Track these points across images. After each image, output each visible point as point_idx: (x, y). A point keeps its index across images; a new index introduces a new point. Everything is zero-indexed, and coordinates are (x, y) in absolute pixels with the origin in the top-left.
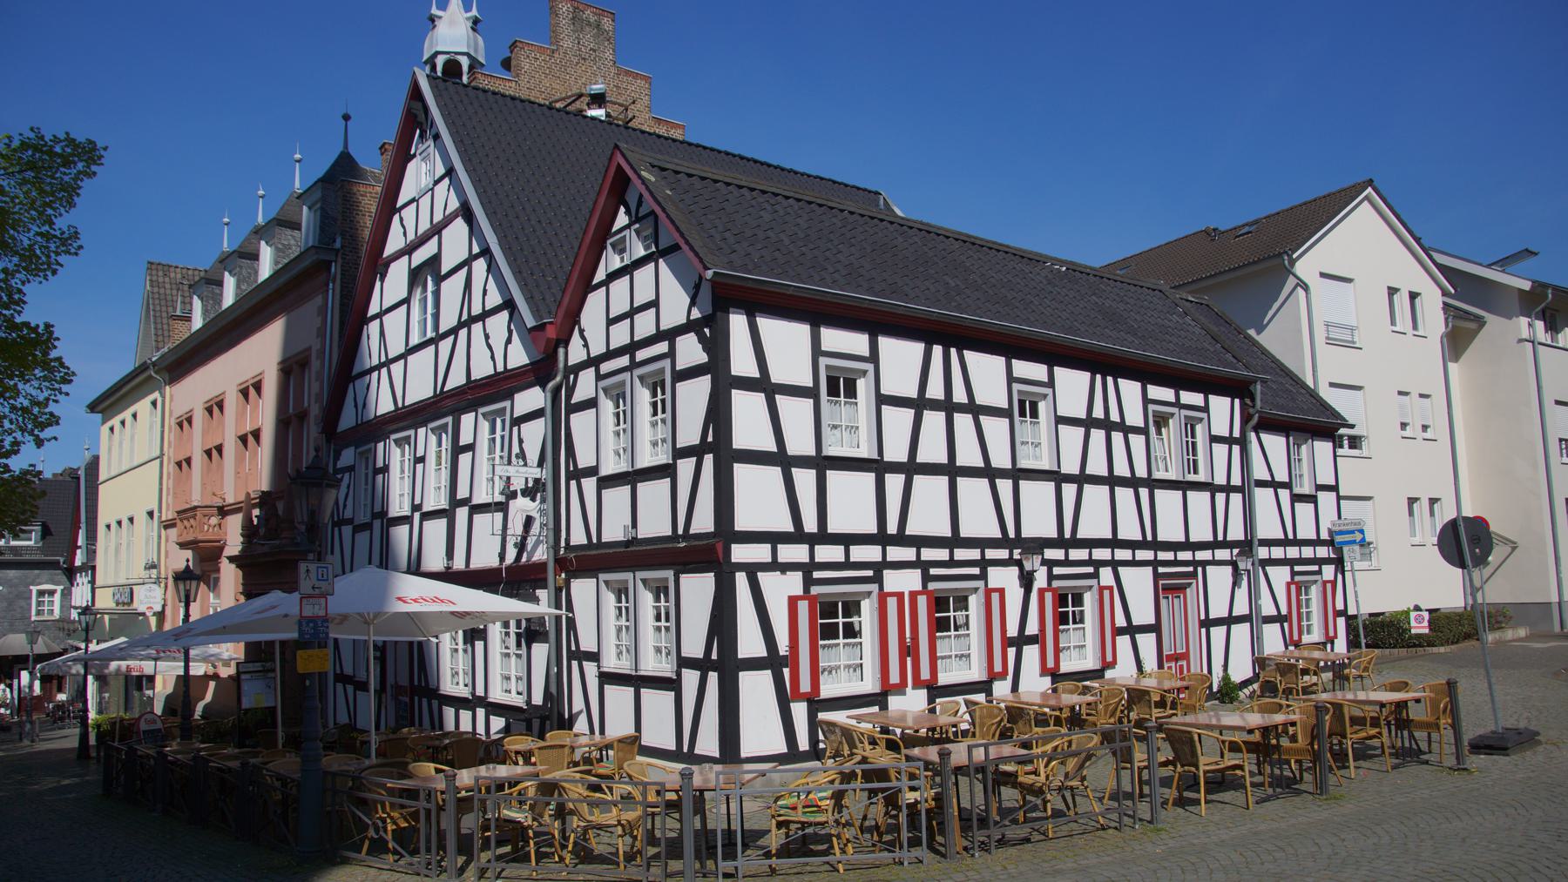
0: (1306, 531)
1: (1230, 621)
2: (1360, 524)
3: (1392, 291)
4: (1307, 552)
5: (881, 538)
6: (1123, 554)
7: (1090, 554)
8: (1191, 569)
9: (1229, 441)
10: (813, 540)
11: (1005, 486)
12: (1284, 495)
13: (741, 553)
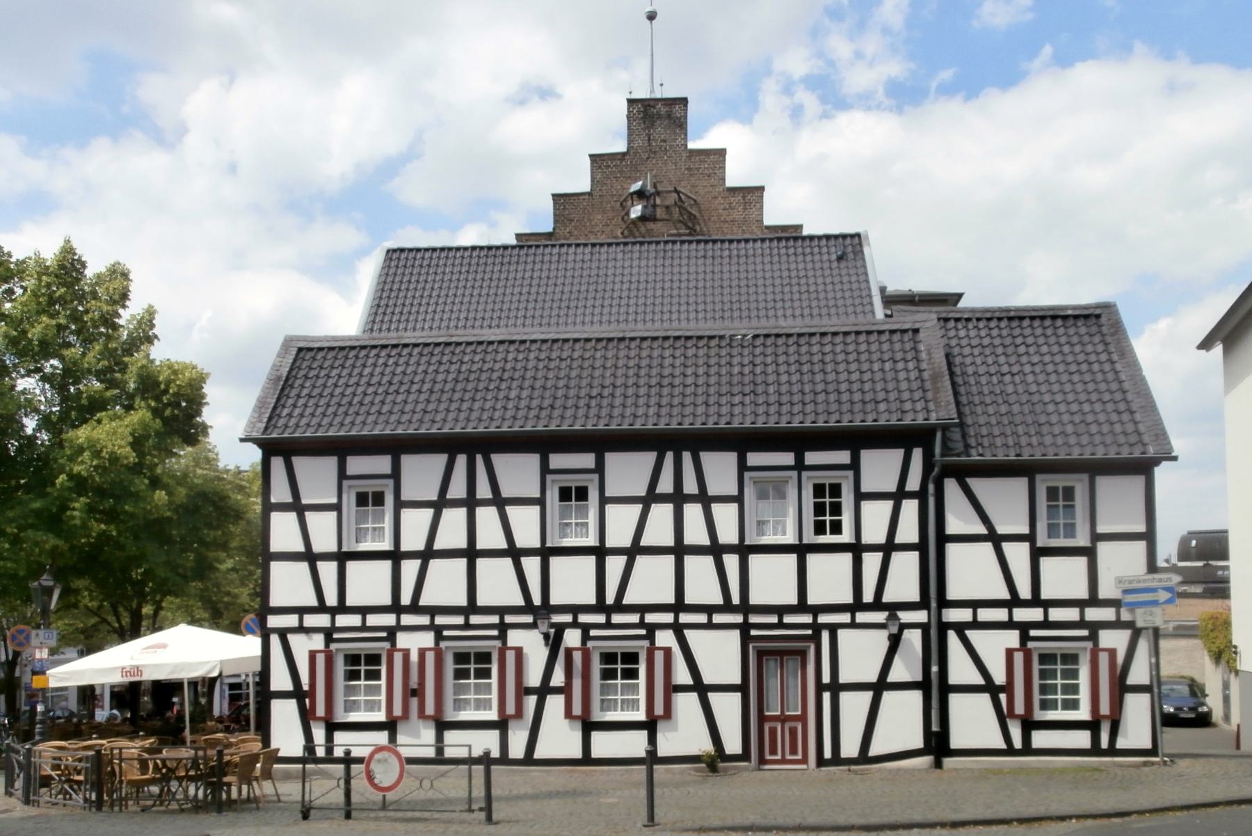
5: (396, 607)
10: (333, 612)
11: (731, 562)
13: (274, 621)
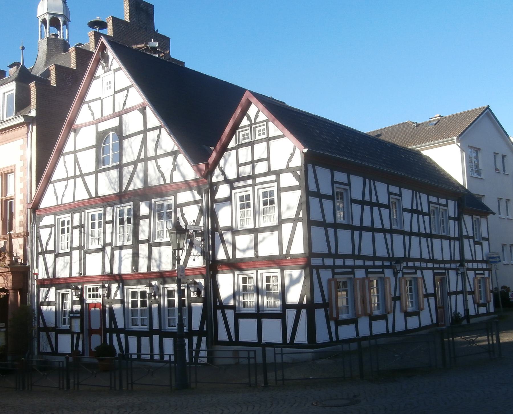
0: (479, 257)
1: (456, 293)
2: (498, 254)
3: (496, 154)
4: (480, 266)
6: (424, 265)
7: (414, 264)
8: (444, 271)
9: (454, 219)
12: (472, 241)
